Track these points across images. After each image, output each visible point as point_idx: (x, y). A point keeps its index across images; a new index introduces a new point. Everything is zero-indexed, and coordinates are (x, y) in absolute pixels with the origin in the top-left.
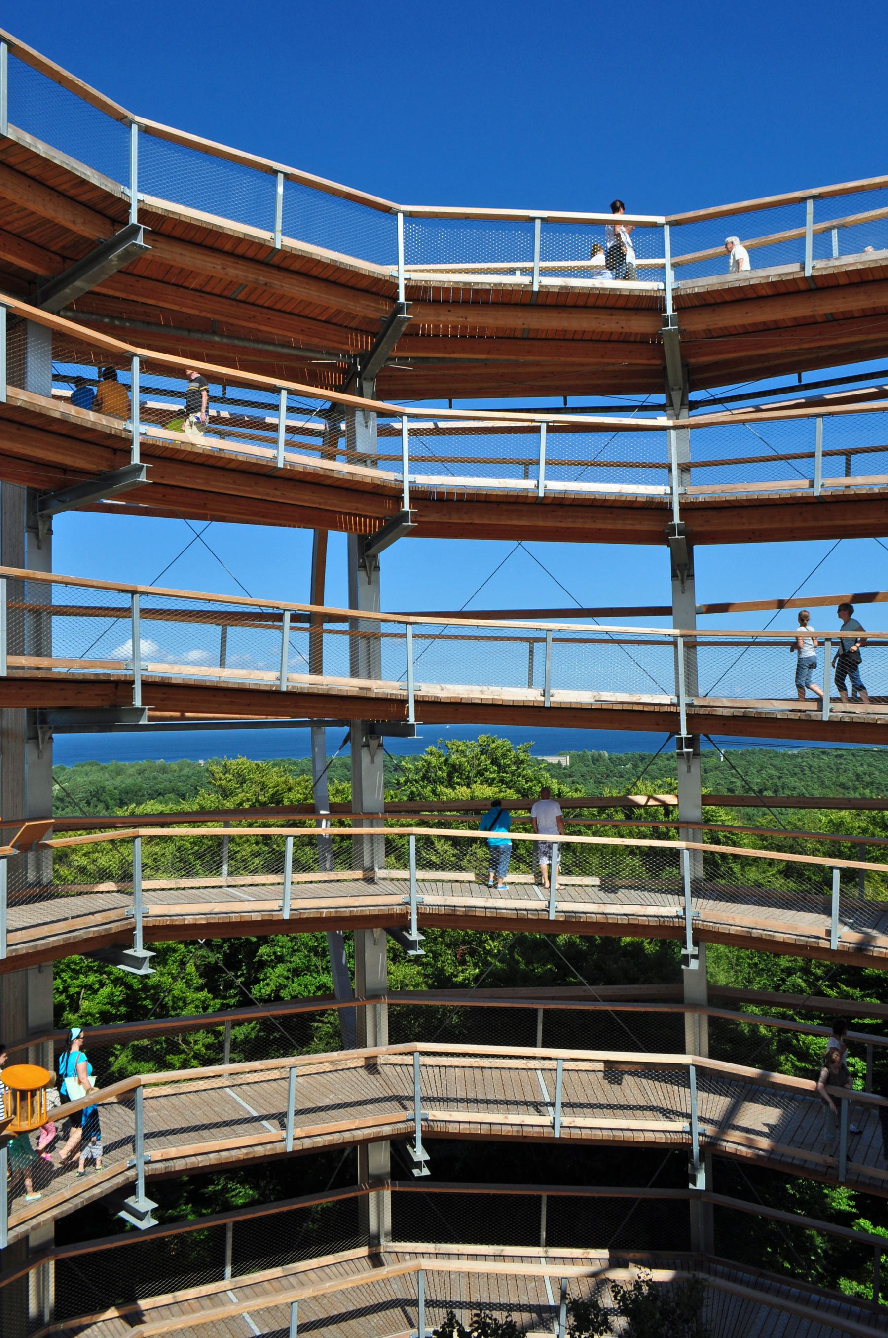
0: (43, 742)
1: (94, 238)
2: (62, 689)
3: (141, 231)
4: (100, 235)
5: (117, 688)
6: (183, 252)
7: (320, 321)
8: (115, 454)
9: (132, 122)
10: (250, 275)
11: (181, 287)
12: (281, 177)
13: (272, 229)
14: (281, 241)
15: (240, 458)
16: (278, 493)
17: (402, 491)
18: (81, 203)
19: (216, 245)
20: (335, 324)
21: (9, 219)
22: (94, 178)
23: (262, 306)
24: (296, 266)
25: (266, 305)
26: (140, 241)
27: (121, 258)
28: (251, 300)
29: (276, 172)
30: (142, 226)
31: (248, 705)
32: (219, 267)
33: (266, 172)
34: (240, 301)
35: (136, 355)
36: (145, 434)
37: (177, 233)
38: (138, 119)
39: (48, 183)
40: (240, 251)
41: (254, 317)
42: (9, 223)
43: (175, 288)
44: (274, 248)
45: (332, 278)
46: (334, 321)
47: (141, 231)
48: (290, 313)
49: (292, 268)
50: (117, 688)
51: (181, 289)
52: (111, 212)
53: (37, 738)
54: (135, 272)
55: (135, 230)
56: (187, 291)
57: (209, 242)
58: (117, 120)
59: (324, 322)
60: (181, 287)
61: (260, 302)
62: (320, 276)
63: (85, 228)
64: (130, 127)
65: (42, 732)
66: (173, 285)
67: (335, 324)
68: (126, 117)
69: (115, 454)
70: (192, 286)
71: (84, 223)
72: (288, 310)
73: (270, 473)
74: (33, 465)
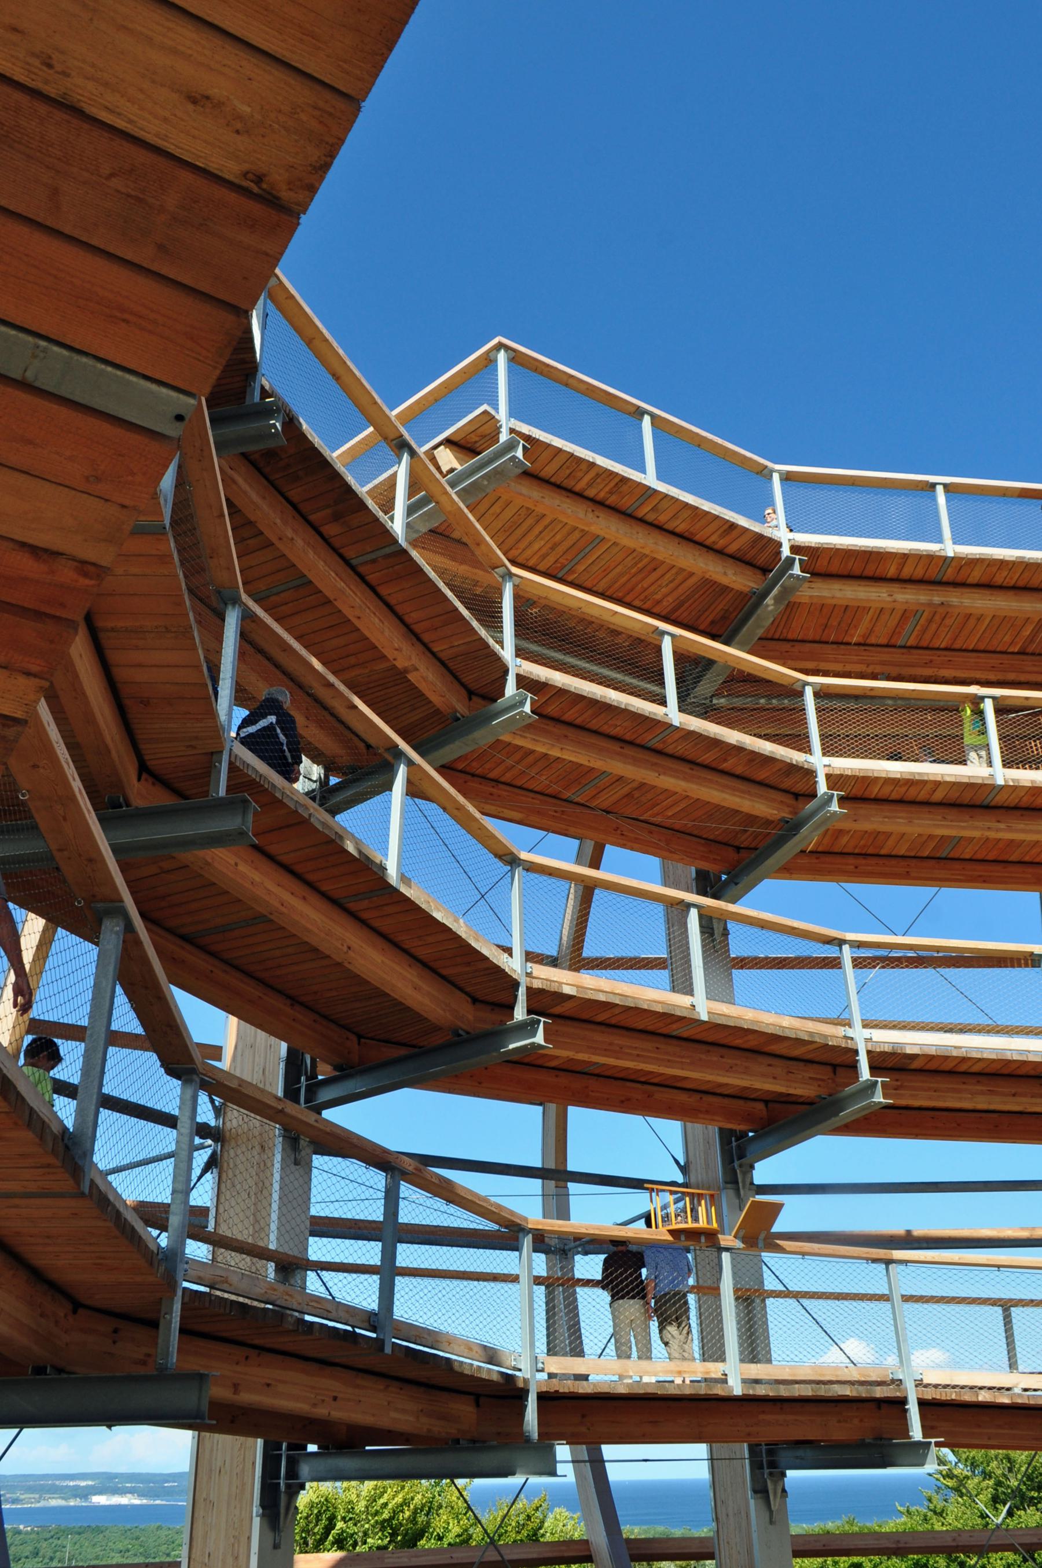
0: (744, 1187)
1: (746, 590)
2: (770, 1065)
3: (797, 562)
4: (753, 585)
5: (835, 1073)
6: (843, 587)
7: (1013, 653)
8: (797, 799)
9: (772, 471)
10: (922, 597)
11: (842, 643)
12: (940, 489)
13: (940, 540)
14: (950, 549)
15: (948, 779)
16: (1002, 826)
17: (856, 1052)
18: (731, 556)
19: (877, 574)
20: (1033, 654)
21: (658, 597)
22: (742, 521)
23: (938, 649)
24: (975, 576)
25: (942, 646)
26: (796, 570)
27: (777, 600)
28: (924, 643)
29: (933, 486)
30: (797, 557)
31: (1014, 1095)
32: (885, 595)
33: (922, 489)
34: (911, 647)
35: (808, 684)
36: (829, 766)
37: (834, 568)
38: (778, 467)
39: (697, 538)
40: (906, 573)
41: (931, 661)
42: (659, 602)
43: (835, 646)
44: (946, 558)
45: (1021, 583)
46: (1030, 650)
47: (797, 562)
48: (973, 651)
49: (970, 581)
50: (835, 1073)
51: (842, 647)
52: (761, 560)
53: (737, 1183)
54: (790, 636)
55: (790, 562)
56: (849, 647)
57: (870, 571)
58: (757, 473)
59: (1018, 653)
60: (842, 643)
61: (936, 643)
62: (1005, 584)
63: (738, 580)
64: (772, 476)
65: (741, 1171)
66: (832, 643)
67: (1033, 654)
68: (766, 467)
69: (797, 799)
70: (854, 640)
71: (735, 574)
72: (971, 648)
73: (985, 803)
74: (703, 841)
